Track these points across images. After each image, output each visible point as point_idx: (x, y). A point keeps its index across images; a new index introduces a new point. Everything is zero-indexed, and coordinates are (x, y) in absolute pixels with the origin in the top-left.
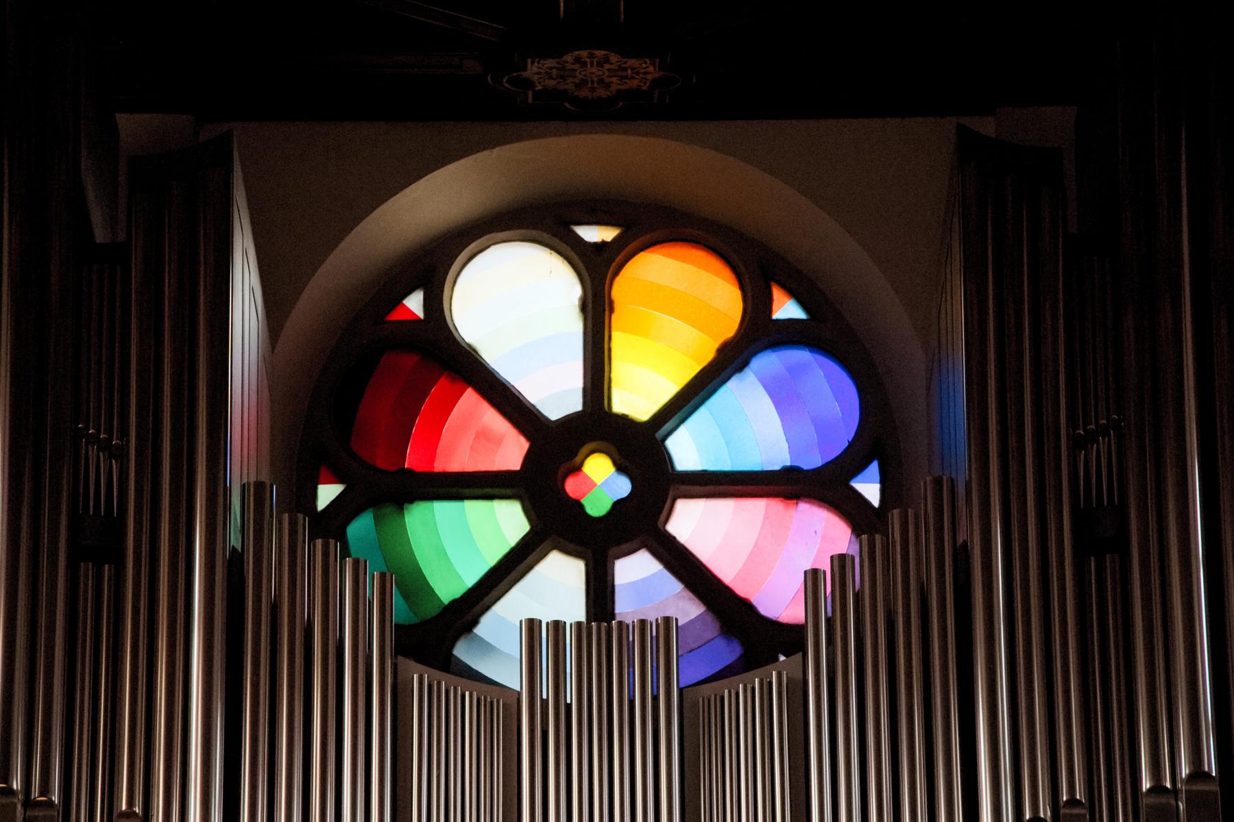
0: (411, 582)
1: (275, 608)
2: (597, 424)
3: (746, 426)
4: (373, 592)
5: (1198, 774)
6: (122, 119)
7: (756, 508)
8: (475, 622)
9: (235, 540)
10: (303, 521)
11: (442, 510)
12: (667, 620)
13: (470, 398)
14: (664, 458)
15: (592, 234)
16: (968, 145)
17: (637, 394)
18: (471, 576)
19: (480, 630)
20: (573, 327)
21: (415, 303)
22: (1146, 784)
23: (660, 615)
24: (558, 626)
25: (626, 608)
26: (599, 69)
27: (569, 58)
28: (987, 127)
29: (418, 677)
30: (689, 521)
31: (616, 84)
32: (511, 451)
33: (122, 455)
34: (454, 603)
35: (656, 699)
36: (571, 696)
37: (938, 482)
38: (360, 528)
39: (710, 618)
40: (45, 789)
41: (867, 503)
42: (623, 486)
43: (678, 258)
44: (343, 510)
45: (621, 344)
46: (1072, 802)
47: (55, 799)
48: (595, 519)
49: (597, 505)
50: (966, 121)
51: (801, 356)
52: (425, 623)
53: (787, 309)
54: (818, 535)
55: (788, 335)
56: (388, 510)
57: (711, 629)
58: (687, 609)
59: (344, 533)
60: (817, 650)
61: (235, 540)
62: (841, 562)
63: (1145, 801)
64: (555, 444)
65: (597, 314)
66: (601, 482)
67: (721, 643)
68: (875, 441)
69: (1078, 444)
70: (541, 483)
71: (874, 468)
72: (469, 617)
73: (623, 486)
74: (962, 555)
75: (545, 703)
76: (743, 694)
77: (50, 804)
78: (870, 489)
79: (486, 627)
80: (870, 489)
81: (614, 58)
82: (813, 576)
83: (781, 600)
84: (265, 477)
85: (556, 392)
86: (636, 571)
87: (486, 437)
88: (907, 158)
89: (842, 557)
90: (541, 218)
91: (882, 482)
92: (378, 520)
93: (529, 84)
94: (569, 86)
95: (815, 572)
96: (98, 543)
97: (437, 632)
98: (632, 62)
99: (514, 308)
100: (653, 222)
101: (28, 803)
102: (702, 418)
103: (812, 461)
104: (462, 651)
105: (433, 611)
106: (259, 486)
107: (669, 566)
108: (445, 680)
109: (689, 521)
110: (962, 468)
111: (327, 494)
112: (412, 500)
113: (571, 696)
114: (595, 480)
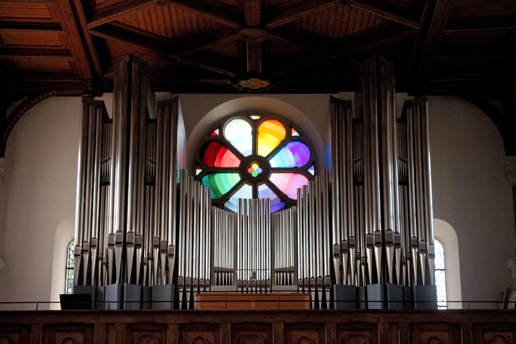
0: (216, 191)
1: (186, 196)
2: (255, 157)
3: (286, 158)
4: (207, 191)
5: (377, 231)
6: (156, 93)
7: (288, 175)
8: (229, 199)
9: (178, 181)
10: (193, 177)
11: (222, 175)
12: (268, 199)
13: (228, 152)
14: (269, 165)
15: (254, 117)
16: (333, 100)
17: (263, 152)
18: (228, 189)
19: (230, 200)
20: (250, 137)
21: (217, 132)
22: (367, 233)
23: (267, 198)
24: (245, 200)
25: (260, 196)
26: (255, 83)
27: (249, 80)
28: (336, 96)
29: (216, 210)
30: (274, 178)
31: (259, 86)
32: (237, 163)
33: (155, 163)
34: (225, 195)
35: (266, 215)
36: (248, 214)
37: (325, 171)
38: (205, 179)
39: (278, 198)
40: (139, 232)
41: (311, 175)
42: (260, 171)
43: (273, 123)
44: (202, 175)
45: (260, 140)
46: (352, 236)
47: (142, 234)
48: (256, 177)
49: (255, 174)
50: (332, 95)
51: (298, 143)
52: (218, 199)
53: (295, 134)
54: (301, 181)
55: (295, 139)
56: (211, 175)
57: (279, 201)
58: (273, 196)
59: (201, 179)
60: (300, 204)
61: (178, 181)
62: (305, 187)
63: (366, 236)
64: (246, 162)
65: (255, 134)
66: (255, 169)
67: (281, 203)
68: (313, 162)
69: (354, 162)
70: (243, 170)
71: (313, 167)
72: (228, 198)
73: (260, 171)
74: (330, 186)
75: (242, 216)
76: (284, 214)
77: (140, 235)
78: (312, 172)
79: (231, 200)
80: (312, 172)
81: (259, 81)
82: (299, 190)
83: (293, 195)
84: (185, 168)
85: (246, 150)
86: (263, 188)
87: (232, 160)
88: (320, 102)
89: (305, 186)
90: (244, 114)
91: (315, 170)
92: (209, 177)
93: (241, 86)
94: (249, 86)
95: (299, 189)
96: (150, 182)
97: (220, 202)
98: (263, 81)
99: (238, 133)
100: (267, 115)
101: (136, 234)
102: (277, 157)
103: (300, 166)
104: (226, 205)
105: (220, 196)
106: (183, 170)
107: (270, 187)
108: (222, 211)
109: (274, 178)
110: (330, 167)
111: (198, 172)
112: (216, 173)
113: (248, 214)
114: (254, 170)
